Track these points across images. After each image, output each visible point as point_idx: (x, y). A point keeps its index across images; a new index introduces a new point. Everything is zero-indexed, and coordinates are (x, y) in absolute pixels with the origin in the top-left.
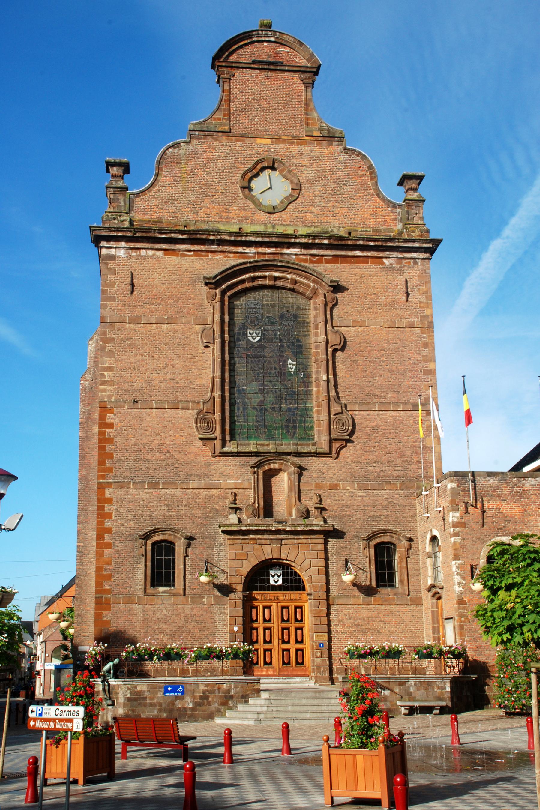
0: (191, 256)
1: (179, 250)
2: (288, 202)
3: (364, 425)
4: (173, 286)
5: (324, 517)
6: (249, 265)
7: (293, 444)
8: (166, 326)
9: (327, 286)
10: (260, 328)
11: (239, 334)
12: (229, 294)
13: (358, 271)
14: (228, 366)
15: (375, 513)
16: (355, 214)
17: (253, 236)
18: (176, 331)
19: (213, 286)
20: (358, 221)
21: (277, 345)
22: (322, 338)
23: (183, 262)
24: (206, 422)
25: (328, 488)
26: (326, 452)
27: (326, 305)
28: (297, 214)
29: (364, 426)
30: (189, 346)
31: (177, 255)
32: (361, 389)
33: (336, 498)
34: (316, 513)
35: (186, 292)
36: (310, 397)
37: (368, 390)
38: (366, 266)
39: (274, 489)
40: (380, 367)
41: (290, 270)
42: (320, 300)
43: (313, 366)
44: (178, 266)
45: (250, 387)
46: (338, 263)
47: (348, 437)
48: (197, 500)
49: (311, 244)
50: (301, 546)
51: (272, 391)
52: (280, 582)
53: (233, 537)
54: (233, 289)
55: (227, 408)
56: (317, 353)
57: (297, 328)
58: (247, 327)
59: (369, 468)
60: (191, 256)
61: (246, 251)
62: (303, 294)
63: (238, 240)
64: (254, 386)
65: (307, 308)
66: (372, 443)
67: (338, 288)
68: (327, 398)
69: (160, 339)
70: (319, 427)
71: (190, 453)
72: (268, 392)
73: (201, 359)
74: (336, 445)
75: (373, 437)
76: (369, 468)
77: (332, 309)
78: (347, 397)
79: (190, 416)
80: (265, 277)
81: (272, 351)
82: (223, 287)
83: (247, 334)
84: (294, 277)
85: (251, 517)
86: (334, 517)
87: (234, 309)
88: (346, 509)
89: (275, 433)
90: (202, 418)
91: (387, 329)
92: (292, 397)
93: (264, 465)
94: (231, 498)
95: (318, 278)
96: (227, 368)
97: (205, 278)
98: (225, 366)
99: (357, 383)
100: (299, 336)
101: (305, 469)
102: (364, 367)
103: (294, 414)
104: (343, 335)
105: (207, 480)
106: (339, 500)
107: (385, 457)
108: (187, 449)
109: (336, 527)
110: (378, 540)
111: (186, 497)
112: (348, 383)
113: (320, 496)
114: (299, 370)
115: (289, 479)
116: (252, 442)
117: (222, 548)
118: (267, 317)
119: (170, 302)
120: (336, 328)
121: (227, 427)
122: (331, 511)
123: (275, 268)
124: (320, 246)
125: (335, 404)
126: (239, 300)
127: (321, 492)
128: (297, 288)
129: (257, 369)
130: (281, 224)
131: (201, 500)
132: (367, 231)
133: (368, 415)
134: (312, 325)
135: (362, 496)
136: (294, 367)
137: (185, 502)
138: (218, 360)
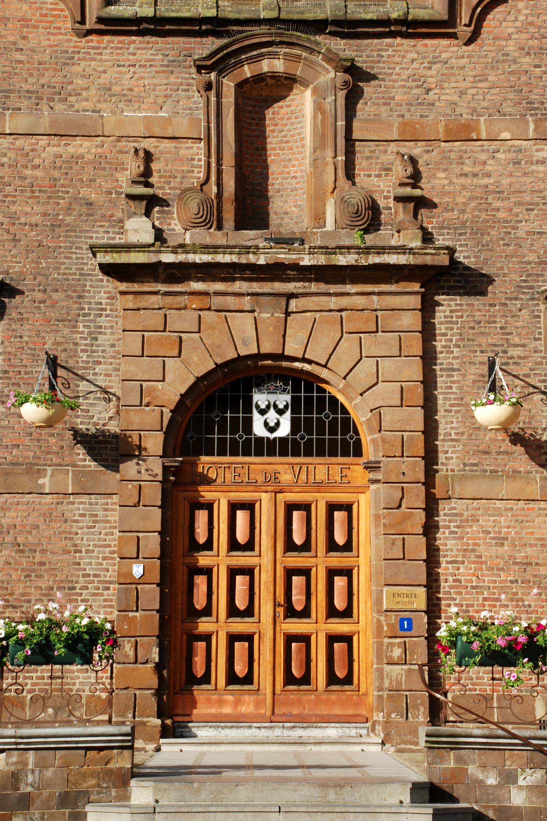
5: (423, 229)
25: (442, 137)
26: (437, 17)
33: (467, 169)
34: (401, 216)
39: (272, 141)
48: (28, 172)
50: (348, 317)
52: (284, 430)
53: (136, 287)
85: (196, 225)
86: (459, 228)
88: (498, 204)
93: (240, 64)
94: (135, 167)
101: (370, 77)
105: (59, 107)
106: (475, 175)
109: (460, 257)
113: (413, 161)
115: (318, 107)
122: (447, 210)
127: (417, 150)
131: (39, 173)
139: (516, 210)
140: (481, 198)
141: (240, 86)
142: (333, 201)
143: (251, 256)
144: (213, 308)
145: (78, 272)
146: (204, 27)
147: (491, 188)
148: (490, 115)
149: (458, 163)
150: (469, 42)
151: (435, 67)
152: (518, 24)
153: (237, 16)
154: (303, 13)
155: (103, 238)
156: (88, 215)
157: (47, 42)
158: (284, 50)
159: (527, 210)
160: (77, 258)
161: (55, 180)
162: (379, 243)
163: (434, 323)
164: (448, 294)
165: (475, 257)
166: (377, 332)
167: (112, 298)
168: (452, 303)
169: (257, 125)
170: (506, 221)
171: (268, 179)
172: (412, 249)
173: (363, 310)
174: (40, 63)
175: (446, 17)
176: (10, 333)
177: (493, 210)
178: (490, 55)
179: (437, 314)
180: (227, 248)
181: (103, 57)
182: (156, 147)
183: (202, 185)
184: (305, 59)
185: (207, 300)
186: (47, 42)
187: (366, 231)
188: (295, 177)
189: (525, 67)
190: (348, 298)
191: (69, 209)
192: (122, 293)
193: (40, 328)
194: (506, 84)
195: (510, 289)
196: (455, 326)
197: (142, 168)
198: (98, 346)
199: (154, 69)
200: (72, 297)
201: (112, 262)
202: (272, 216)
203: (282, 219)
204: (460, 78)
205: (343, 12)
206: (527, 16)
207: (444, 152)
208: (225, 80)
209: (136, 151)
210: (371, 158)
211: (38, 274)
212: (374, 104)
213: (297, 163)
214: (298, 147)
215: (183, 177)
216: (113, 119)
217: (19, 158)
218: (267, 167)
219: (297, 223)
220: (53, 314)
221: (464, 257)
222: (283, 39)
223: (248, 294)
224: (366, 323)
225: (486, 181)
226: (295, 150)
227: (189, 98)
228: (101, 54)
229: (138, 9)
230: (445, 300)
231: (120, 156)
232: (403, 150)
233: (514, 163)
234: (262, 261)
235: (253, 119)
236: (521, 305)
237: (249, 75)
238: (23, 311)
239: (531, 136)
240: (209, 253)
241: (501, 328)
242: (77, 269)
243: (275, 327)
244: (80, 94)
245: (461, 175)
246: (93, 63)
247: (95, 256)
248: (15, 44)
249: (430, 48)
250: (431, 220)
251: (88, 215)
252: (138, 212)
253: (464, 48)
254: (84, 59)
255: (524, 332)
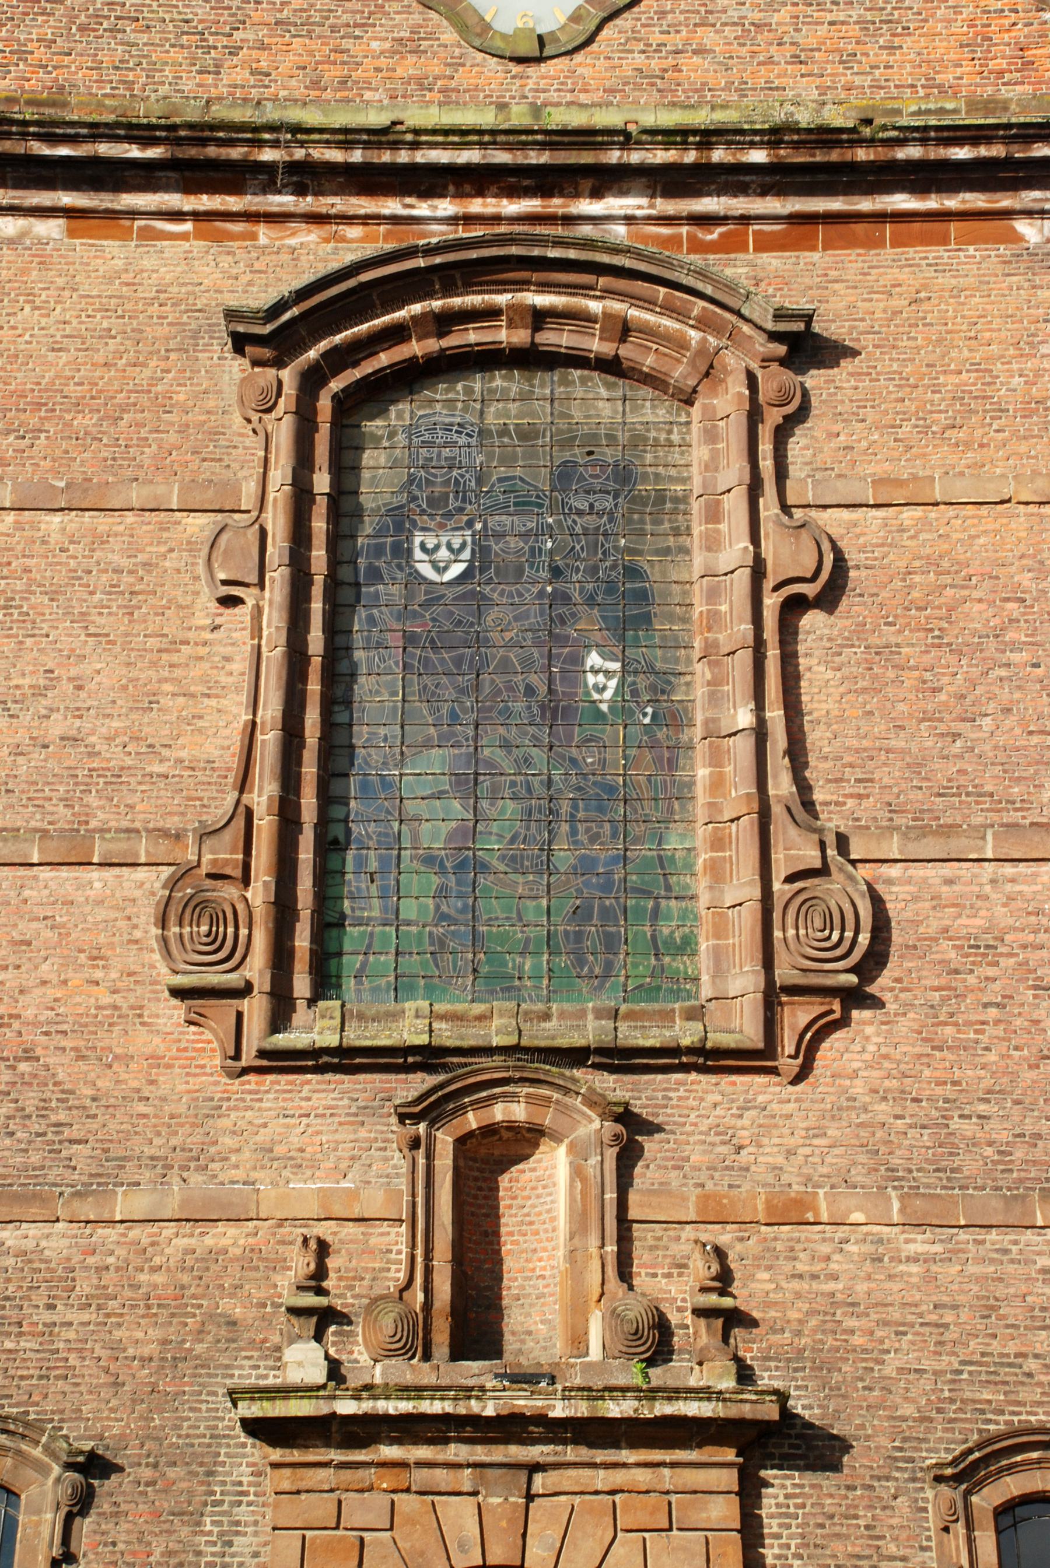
0: (184, 236)
1: (133, 214)
2: (603, 15)
3: (932, 927)
4: (99, 358)
5: (738, 1360)
6: (421, 262)
7: (599, 1014)
8: (57, 518)
9: (760, 338)
10: (470, 524)
11: (378, 551)
12: (336, 385)
13: (904, 275)
14: (319, 684)
15: (995, 1346)
16: (891, 48)
17: (444, 146)
18: (101, 540)
19: (266, 353)
20: (905, 74)
21: (542, 594)
22: (736, 550)
23: (146, 263)
24: (205, 919)
25: (761, 1217)
26: (748, 1045)
27: (754, 416)
28: (639, 59)
29: (931, 931)
30: (152, 600)
31: (125, 235)
32: (916, 767)
33: (801, 1267)
34: (704, 1339)
35: (154, 381)
36: (683, 807)
37: (943, 771)
38: (935, 252)
39: (509, 1223)
40: (1003, 672)
41: (603, 281)
42: (728, 399)
43: (698, 678)
44: (127, 277)
45: (415, 780)
46: (814, 248)
47: (853, 979)
48: (143, 1277)
49: (696, 168)
50: (625, 1504)
51: (513, 784)
53: (296, 1455)
54: (355, 364)
55: (306, 854)
56: (713, 620)
57: (630, 521)
58: (414, 523)
59: (956, 1124)
60: (184, 236)
61: (415, 212)
62: (653, 380)
63: (381, 167)
64: (436, 762)
65: (675, 438)
66: (968, 1010)
67: (804, 346)
68: (755, 806)
69: (27, 570)
70: (717, 936)
71: (126, 1059)
72: (495, 789)
73: (202, 651)
74: (797, 1016)
75: (972, 980)
76: (956, 1124)
77: (782, 434)
78: (850, 803)
79: (138, 893)
80: (492, 313)
81: (516, 619)
82: (312, 354)
83: (410, 551)
84: (617, 306)
85: (391, 1354)
86: (794, 1360)
87: (360, 449)
88: (851, 1323)
89: (521, 968)
90: (189, 904)
91: (1031, 508)
92: (601, 810)
93: (462, 1110)
94: (302, 1264)
95: (724, 306)
96: (314, 687)
97: (232, 315)
98: (304, 679)
99: (893, 743)
100: (639, 553)
101: (652, 1128)
102: (928, 676)
103: (607, 887)
104: (832, 541)
105: (196, 1179)
106: (814, 1277)
107: (1033, 1074)
108: (114, 1040)
109: (797, 1406)
110: (1013, 1486)
111: (91, 1260)
112: (855, 743)
113: (720, 1253)
114: (635, 693)
115: (577, 1172)
116: (410, 1006)
117: (243, 1513)
118: (500, 480)
119: (85, 421)
120: (798, 513)
121: (302, 941)
122: (774, 1331)
123: (535, 277)
124: (735, 179)
125: (793, 831)
126: (383, 412)
127: (725, 1237)
128: (631, 355)
129: (450, 693)
130: (569, 104)
131: (159, 1278)
132: (942, 111)
133: (949, 882)
134: (696, 507)
135: (929, 1259)
136: (613, 683)
137: (84, 1287)
138: (274, 655)
139: (879, 1334)
140: (826, 1313)
141: (461, 1142)
142: (599, 1314)
143: (473, 1402)
144: (414, 1488)
145: (208, 1433)
146: (410, 1060)
147: (839, 1297)
148: (832, 1187)
149: (786, 1258)
150: (797, 1080)
151: (747, 1114)
152: (867, 1056)
153: (458, 1043)
154: (553, 1038)
155: (250, 1376)
156: (228, 1341)
157: (184, 1087)
158: (526, 1090)
159: (897, 1333)
160: (208, 1410)
161: (183, 1287)
162: (671, 1383)
163: (760, 1517)
164: (781, 1468)
165: (820, 1406)
166: (670, 1529)
167: (259, 1474)
168: (788, 1483)
169: (486, 1198)
170: (865, 1351)
171: (501, 1279)
172: (720, 1392)
173: (647, 1492)
174: (172, 1117)
175: (761, 1045)
176: (98, 1538)
177: (845, 1332)
178: (829, 1099)
179: (765, 1501)
180: (436, 1391)
181: (264, 1105)
182: (335, 1234)
183: (401, 1291)
184: (558, 1102)
185: (404, 1474)
186: (184, 1087)
187: (651, 1362)
188: (543, 1277)
189: (881, 1118)
190: (624, 1471)
191: (200, 1332)
192: (275, 1466)
193: (145, 1527)
194: (853, 1141)
195: (878, 1462)
196: (794, 1522)
197: (313, 1266)
198: (233, 1555)
199: (337, 1119)
200: (196, 1474)
201: (260, 1414)
202: (507, 1337)
203: (523, 1342)
204: (786, 1131)
205: (611, 1037)
206: (879, 1045)
207: (765, 1240)
208: (439, 1134)
209: (305, 1241)
210: (656, 1247)
211: (148, 1437)
212: (659, 1167)
213: (545, 1255)
214: (546, 1231)
215: (374, 1279)
216: (273, 1193)
217: (131, 1256)
218: (500, 1262)
219: (545, 1348)
220: (166, 1504)
221: (804, 1407)
222: (525, 1075)
223: (469, 1466)
224: (652, 1514)
225: (831, 1286)
226: (543, 1236)
227: (386, 1159)
228: (261, 1100)
229: (316, 1037)
230: (775, 1477)
231: (281, 1248)
232: (704, 1237)
233: (873, 1260)
234: (490, 1411)
235: (480, 1189)
236: (897, 1489)
237: (474, 1126)
238: (120, 1499)
239: (896, 1218)
240: (409, 1399)
241: (867, 1527)
242: (208, 1428)
243: (509, 1521)
244: (227, 1159)
245: (793, 1276)
246: (249, 1114)
247: (235, 1406)
248: (138, 1091)
249: (740, 1088)
250: (750, 1347)
251: (228, 1341)
252: (305, 1334)
253: (790, 1088)
254: (236, 1108)
255: (904, 1535)
